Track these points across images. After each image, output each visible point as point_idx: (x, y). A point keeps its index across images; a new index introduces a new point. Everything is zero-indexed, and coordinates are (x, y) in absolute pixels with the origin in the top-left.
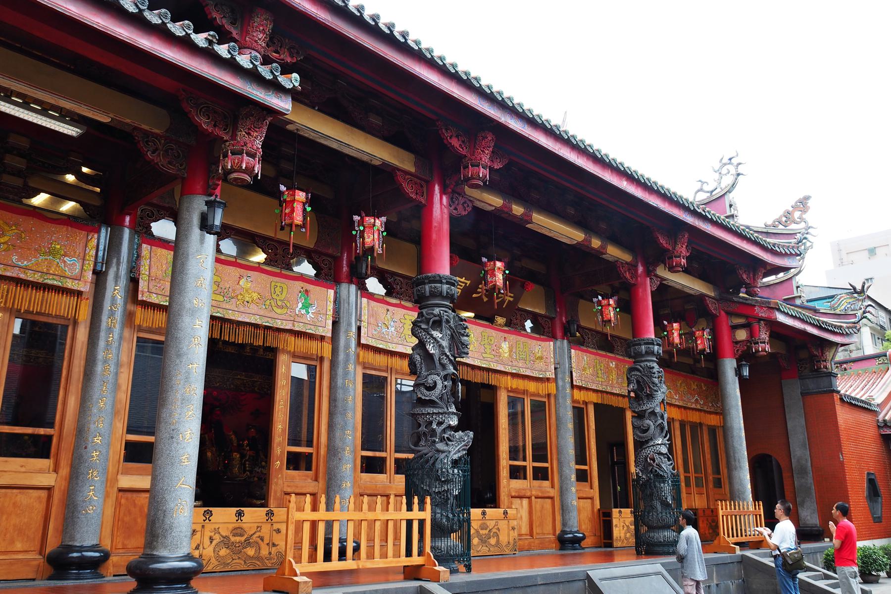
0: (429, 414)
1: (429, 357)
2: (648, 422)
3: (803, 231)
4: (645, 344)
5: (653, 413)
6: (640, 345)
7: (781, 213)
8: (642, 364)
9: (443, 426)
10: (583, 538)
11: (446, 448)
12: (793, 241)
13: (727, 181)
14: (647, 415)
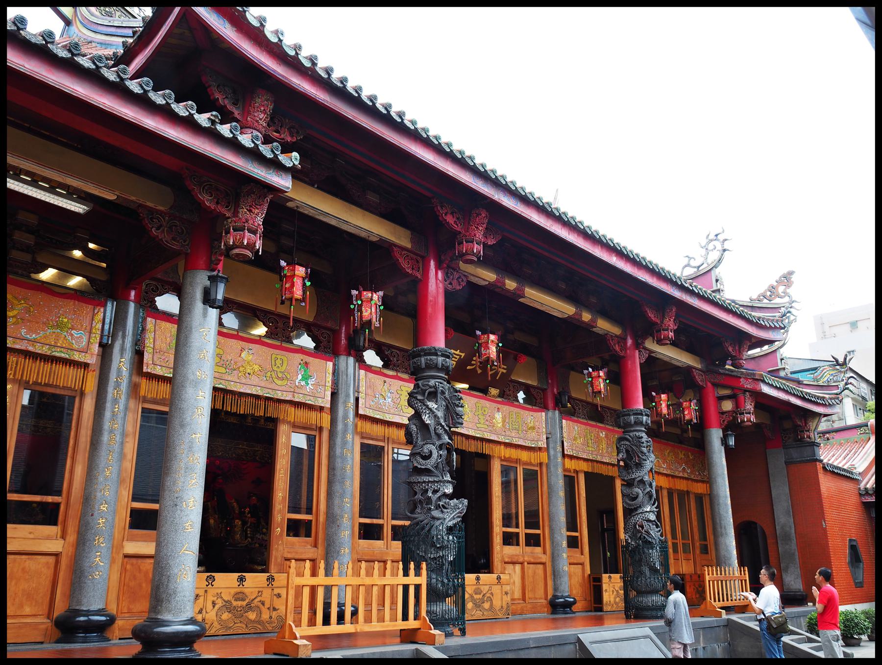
0: (424, 482)
1: (425, 427)
2: (637, 490)
3: (787, 305)
4: (634, 414)
5: (642, 482)
6: (629, 415)
7: (766, 287)
8: (631, 434)
9: (439, 494)
10: (574, 603)
11: (441, 515)
12: (777, 314)
13: (714, 256)
14: (636, 483)
